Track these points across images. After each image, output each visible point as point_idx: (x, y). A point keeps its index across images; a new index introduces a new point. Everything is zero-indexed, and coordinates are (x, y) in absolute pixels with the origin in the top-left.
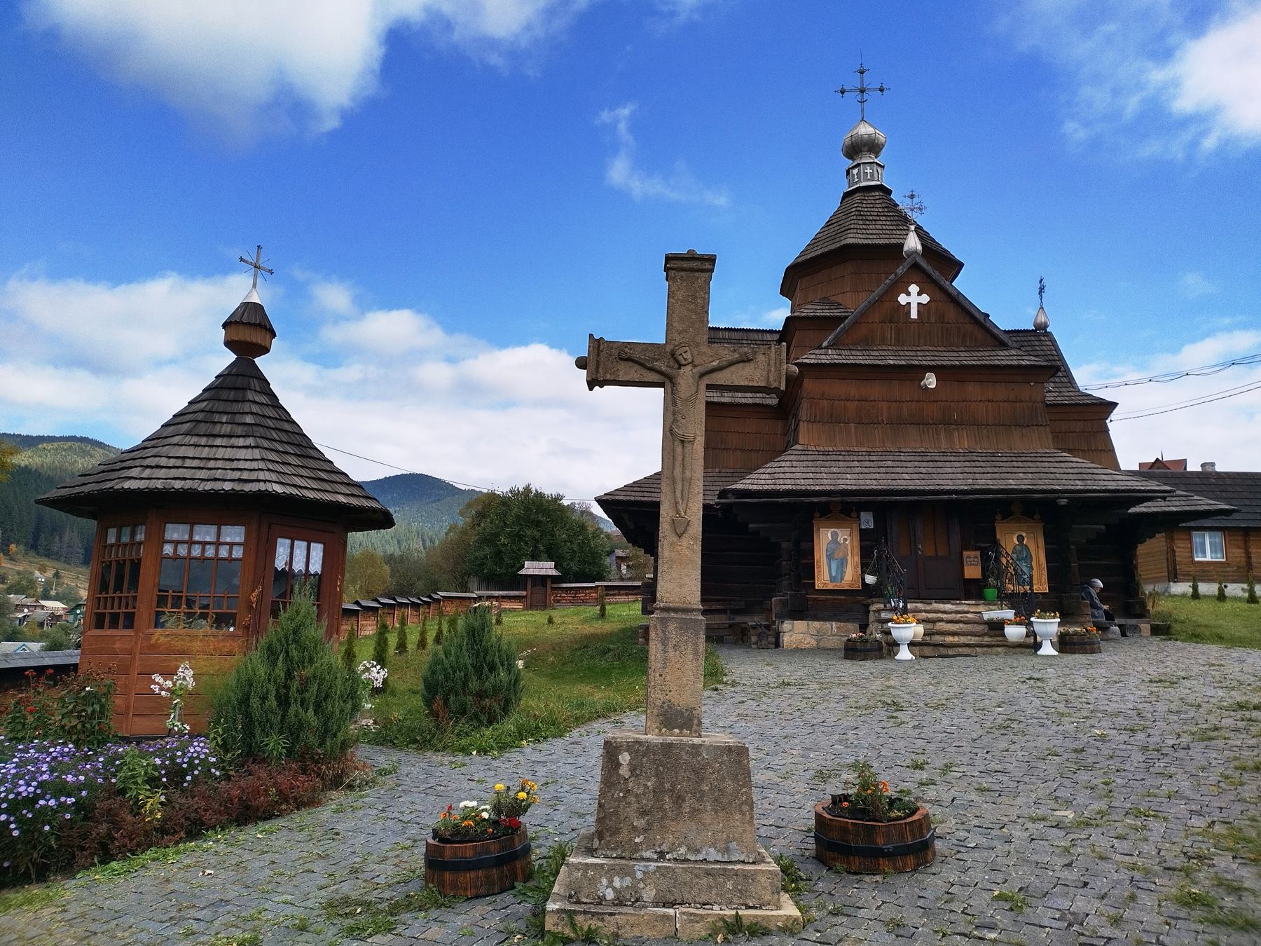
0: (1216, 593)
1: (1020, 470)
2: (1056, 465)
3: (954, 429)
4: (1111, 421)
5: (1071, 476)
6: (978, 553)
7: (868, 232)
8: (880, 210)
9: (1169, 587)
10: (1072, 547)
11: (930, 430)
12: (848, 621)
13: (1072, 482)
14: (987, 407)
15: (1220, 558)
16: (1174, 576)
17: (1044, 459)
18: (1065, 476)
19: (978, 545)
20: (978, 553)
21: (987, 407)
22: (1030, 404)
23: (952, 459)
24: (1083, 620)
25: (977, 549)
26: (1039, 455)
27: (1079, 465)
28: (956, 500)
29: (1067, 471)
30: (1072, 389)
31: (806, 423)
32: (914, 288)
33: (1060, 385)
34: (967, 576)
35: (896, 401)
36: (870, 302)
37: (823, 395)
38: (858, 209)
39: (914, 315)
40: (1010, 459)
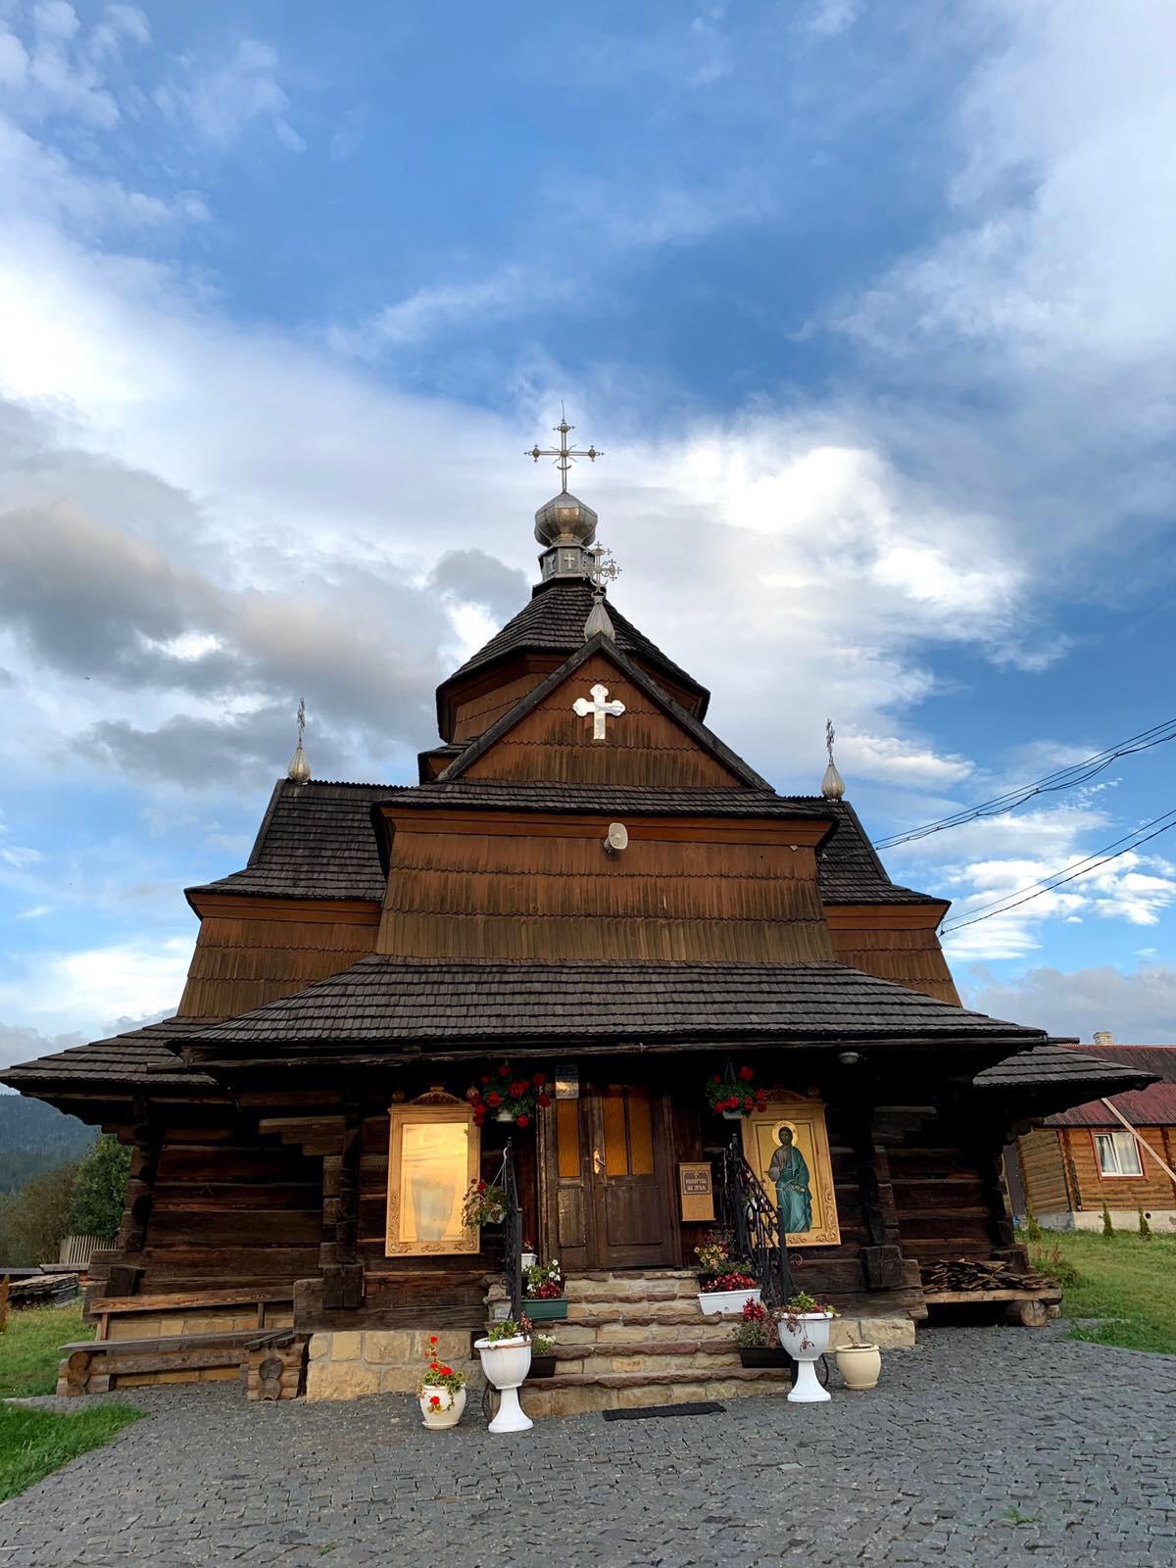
0: (1137, 1227)
1: (773, 998)
2: (839, 989)
3: (662, 926)
4: (942, 933)
5: (864, 1009)
6: (706, 1167)
7: (557, 633)
8: (582, 608)
9: (1071, 1219)
10: (879, 1150)
11: (621, 930)
12: (448, 1325)
13: (862, 1019)
14: (719, 887)
15: (1133, 1171)
16: (1076, 1202)
17: (817, 979)
18: (852, 1009)
19: (708, 1149)
20: (706, 1167)
21: (719, 887)
22: (793, 883)
23: (654, 978)
24: (907, 1300)
25: (706, 1157)
26: (810, 972)
27: (875, 989)
28: (646, 1054)
29: (854, 999)
30: (879, 882)
31: (392, 914)
32: (599, 692)
33: (861, 875)
34: (687, 1217)
35: (561, 875)
36: (523, 708)
37: (429, 861)
38: (549, 605)
39: (599, 734)
40: (757, 979)
